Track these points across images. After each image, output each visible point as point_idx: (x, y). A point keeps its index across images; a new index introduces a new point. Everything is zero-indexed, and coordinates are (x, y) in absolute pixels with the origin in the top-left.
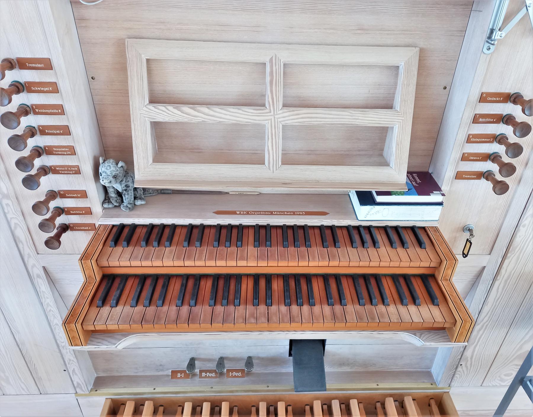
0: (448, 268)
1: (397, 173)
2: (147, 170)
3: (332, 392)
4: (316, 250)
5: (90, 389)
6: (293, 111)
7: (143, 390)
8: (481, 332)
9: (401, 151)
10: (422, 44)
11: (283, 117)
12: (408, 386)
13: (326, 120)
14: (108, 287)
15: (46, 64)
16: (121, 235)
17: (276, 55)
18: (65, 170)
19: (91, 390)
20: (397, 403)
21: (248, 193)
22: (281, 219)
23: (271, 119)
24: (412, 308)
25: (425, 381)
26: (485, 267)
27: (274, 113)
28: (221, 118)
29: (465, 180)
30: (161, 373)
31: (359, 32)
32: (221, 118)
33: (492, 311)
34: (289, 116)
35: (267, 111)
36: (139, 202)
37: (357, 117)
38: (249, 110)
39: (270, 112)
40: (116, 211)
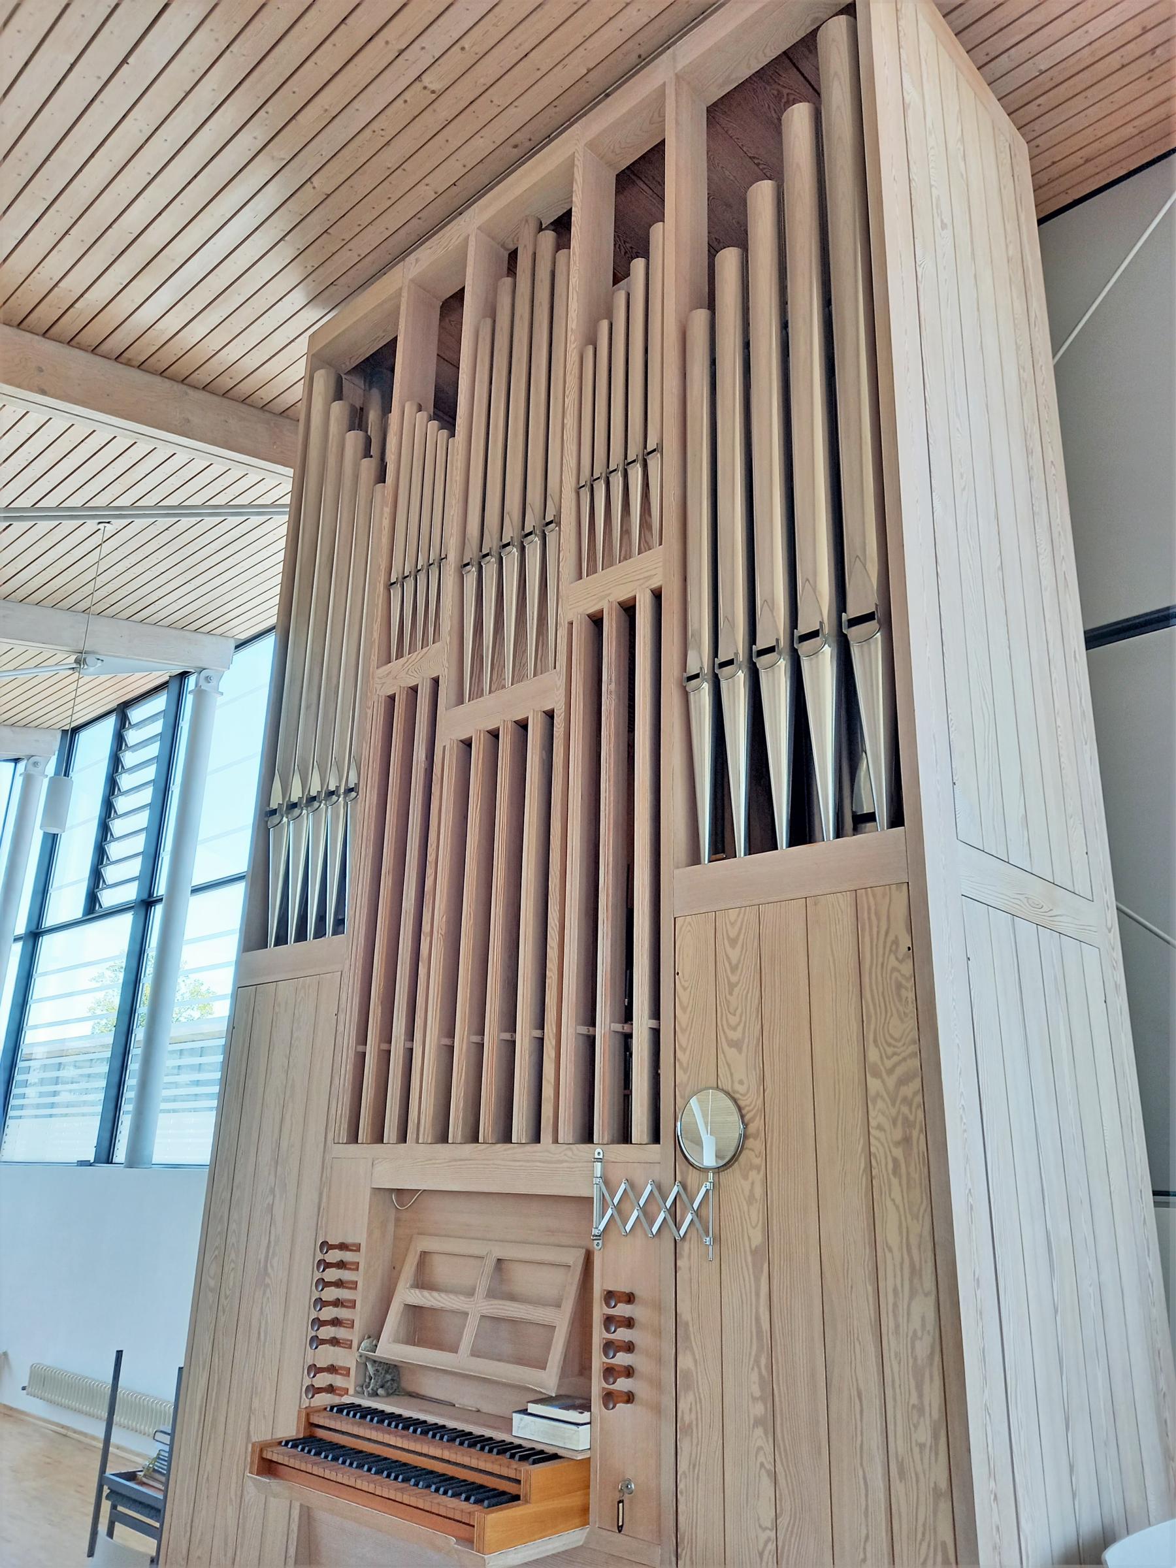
1: (549, 1380)
15: (357, 1248)
36: (380, 1391)
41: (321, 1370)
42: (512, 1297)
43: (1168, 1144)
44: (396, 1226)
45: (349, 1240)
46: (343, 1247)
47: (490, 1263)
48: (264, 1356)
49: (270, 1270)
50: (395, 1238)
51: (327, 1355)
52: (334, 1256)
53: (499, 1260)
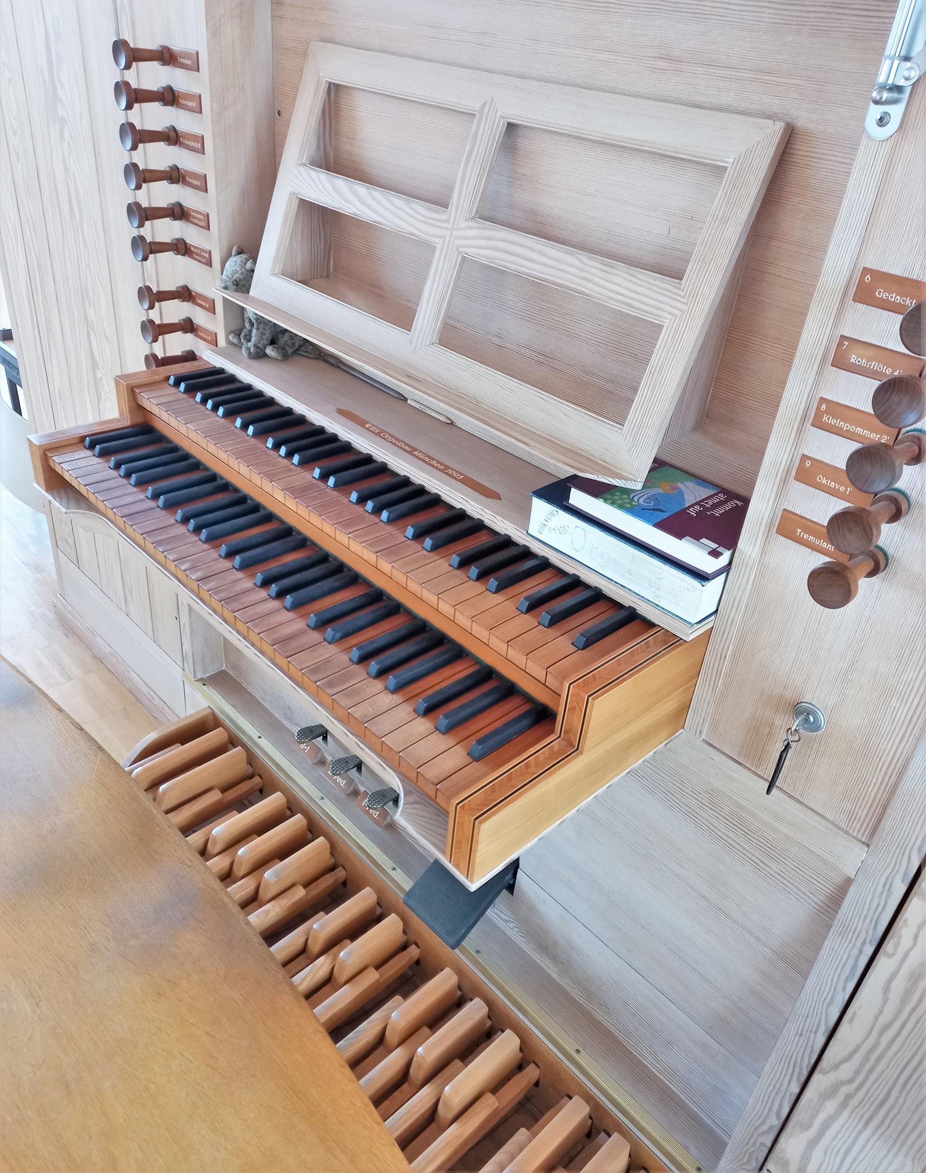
0: (573, 709)
1: (629, 448)
2: (278, 294)
3: (491, 986)
4: (443, 565)
5: (199, 676)
6: (484, 229)
7: (248, 728)
8: (831, 1106)
9: (653, 391)
10: (803, 121)
11: (465, 238)
12: (638, 1118)
13: (533, 265)
14: (136, 447)
16: (211, 385)
17: (493, 98)
18: (197, 254)
19: (201, 680)
20: (590, 1121)
21: (428, 411)
22: (404, 460)
23: (445, 237)
24: (423, 725)
25: (693, 1150)
26: (849, 882)
27: (453, 226)
28: (377, 213)
29: (803, 548)
30: (286, 723)
31: (661, 64)
32: (377, 213)
33: (866, 1058)
34: (474, 238)
35: (444, 217)
36: (269, 351)
37: (589, 276)
38: (420, 208)
39: (448, 221)
40: (232, 350)
41: (163, 296)
42: (539, 228)
43: (292, 113)
44: (276, 18)
45: (177, 45)
46: (166, 57)
47: (488, 133)
48: (85, 244)
49: (61, 93)
50: (276, 46)
51: (170, 271)
52: (150, 76)
53: (510, 125)
